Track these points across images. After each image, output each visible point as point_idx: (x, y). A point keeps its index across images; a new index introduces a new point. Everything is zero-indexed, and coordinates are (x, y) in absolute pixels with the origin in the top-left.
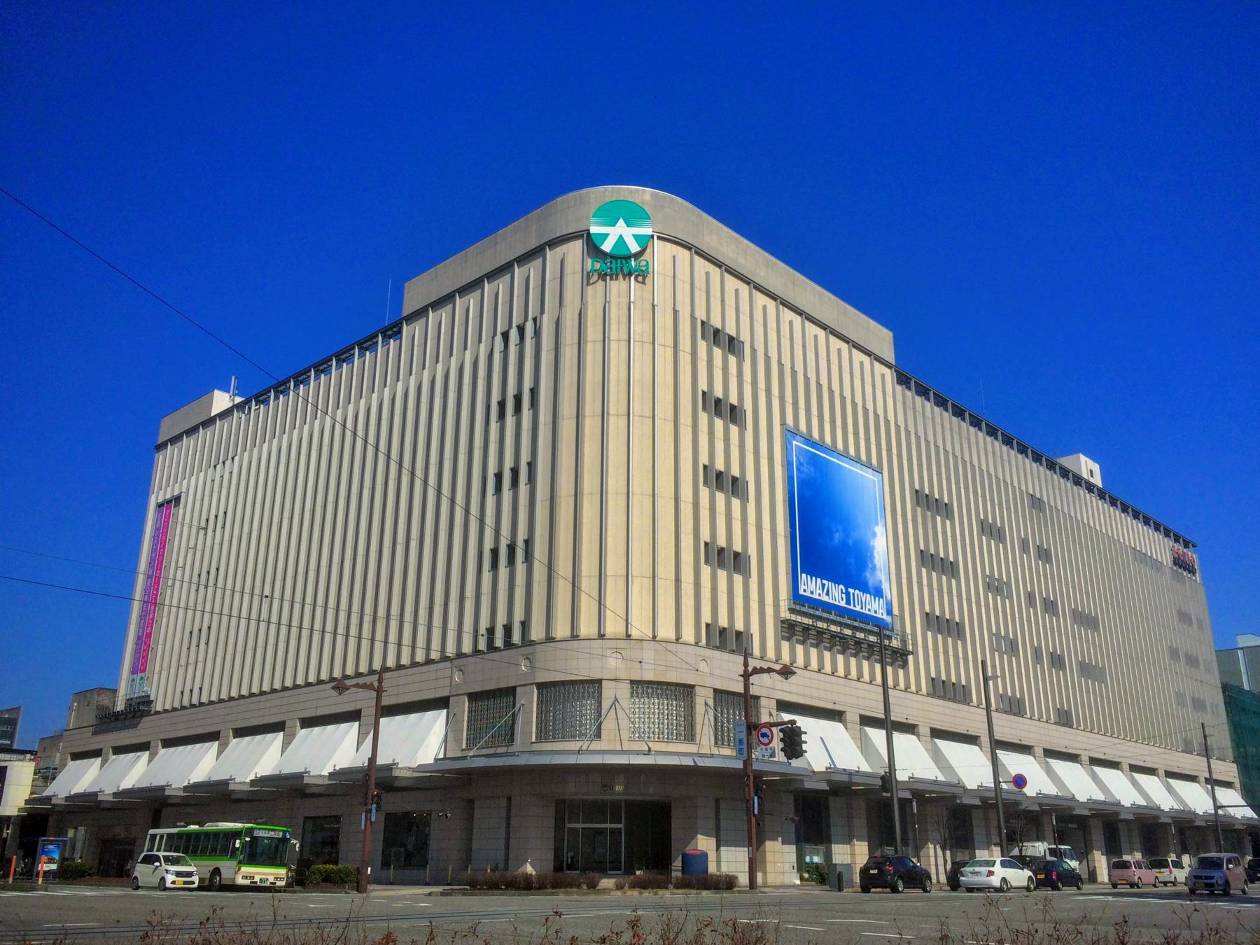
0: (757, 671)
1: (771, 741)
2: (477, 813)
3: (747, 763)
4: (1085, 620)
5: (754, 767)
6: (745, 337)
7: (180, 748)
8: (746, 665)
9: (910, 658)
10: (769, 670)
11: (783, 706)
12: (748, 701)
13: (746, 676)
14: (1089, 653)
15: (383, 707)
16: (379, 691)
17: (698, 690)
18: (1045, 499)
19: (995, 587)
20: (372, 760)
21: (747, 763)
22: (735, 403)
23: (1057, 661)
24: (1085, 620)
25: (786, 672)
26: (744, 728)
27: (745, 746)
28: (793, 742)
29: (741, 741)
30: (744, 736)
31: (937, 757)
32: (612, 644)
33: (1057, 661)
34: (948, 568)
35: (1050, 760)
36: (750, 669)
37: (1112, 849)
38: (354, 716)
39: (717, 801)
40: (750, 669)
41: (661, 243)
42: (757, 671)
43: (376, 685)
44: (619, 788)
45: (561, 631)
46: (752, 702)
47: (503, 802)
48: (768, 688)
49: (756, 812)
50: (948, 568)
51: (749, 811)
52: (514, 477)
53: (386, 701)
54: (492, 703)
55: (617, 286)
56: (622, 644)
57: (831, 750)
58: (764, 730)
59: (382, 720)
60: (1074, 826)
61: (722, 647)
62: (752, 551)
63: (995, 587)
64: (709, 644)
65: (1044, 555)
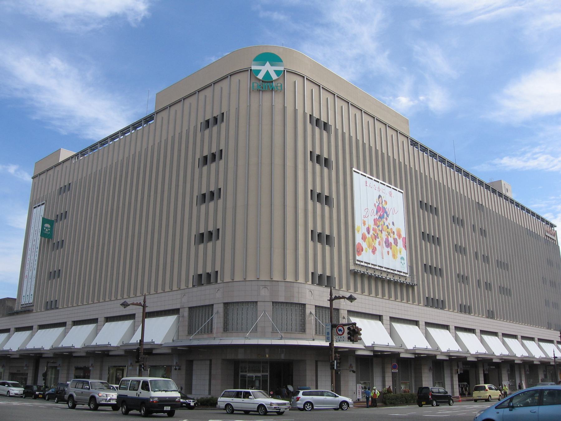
0: (336, 298)
1: (343, 333)
2: (195, 367)
3: (331, 344)
4: (501, 265)
5: (335, 345)
6: (331, 122)
7: (52, 329)
8: (331, 294)
9: (416, 287)
10: (343, 297)
11: (351, 313)
12: (333, 312)
13: (331, 300)
14: (503, 282)
15: (146, 313)
16: (144, 307)
17: (307, 306)
18: (484, 204)
19: (460, 250)
20: (142, 341)
21: (331, 344)
22: (326, 157)
23: (488, 286)
24: (501, 265)
25: (351, 299)
26: (330, 327)
27: (330, 336)
28: (354, 333)
29: (328, 333)
30: (330, 331)
31: (428, 336)
32: (263, 283)
33: (488, 286)
34: (436, 241)
35: (483, 336)
36: (333, 297)
37: (512, 377)
38: (131, 317)
39: (316, 362)
40: (333, 297)
41: (289, 74)
42: (336, 298)
43: (142, 303)
44: (267, 356)
45: (238, 277)
46: (334, 313)
47: (208, 362)
48: (344, 306)
49: (335, 368)
50: (436, 241)
51: (332, 368)
52: (55, 275)
53: (147, 310)
54: (198, 316)
55: (266, 97)
56: (268, 283)
57: (374, 335)
58: (340, 328)
59: (147, 320)
60: (494, 367)
61: (320, 284)
62: (335, 234)
63: (463, 279)
64: (313, 283)
65: (483, 232)
